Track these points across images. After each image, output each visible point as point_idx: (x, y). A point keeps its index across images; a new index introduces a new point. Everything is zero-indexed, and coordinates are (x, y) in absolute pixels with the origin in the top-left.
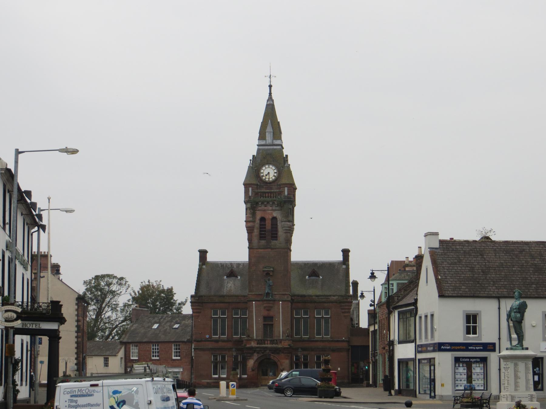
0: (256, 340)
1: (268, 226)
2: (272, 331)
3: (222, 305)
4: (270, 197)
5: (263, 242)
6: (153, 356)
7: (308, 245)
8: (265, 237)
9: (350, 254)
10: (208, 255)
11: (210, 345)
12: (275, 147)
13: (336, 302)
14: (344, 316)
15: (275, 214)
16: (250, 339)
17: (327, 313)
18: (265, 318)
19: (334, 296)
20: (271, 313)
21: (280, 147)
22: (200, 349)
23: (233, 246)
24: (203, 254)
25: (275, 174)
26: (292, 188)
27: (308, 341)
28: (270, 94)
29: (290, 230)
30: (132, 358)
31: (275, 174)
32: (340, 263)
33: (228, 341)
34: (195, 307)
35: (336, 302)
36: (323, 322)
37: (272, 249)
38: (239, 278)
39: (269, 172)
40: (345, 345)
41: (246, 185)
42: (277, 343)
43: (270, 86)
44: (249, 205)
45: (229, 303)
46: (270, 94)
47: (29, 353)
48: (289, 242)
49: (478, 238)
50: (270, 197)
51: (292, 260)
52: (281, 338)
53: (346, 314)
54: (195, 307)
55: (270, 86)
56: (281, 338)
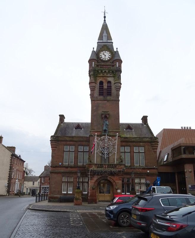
0: (96, 164)
3: (71, 142)
4: (105, 72)
5: (102, 97)
6: (48, 187)
7: (128, 114)
8: (103, 94)
9: (148, 118)
13: (149, 142)
14: (154, 151)
19: (146, 138)
21: (112, 44)
22: (55, 172)
23: (81, 112)
24: (62, 117)
25: (110, 57)
26: (120, 61)
28: (105, 20)
29: (118, 89)
31: (110, 57)
32: (142, 125)
34: (53, 144)
35: (148, 142)
38: (83, 129)
39: (106, 56)
41: (90, 61)
43: (105, 17)
44: (92, 73)
45: (76, 141)
46: (105, 20)
47: (22, 188)
48: (118, 95)
50: (105, 72)
51: (120, 122)
52: (115, 163)
54: (53, 144)
55: (105, 17)
56: (115, 163)
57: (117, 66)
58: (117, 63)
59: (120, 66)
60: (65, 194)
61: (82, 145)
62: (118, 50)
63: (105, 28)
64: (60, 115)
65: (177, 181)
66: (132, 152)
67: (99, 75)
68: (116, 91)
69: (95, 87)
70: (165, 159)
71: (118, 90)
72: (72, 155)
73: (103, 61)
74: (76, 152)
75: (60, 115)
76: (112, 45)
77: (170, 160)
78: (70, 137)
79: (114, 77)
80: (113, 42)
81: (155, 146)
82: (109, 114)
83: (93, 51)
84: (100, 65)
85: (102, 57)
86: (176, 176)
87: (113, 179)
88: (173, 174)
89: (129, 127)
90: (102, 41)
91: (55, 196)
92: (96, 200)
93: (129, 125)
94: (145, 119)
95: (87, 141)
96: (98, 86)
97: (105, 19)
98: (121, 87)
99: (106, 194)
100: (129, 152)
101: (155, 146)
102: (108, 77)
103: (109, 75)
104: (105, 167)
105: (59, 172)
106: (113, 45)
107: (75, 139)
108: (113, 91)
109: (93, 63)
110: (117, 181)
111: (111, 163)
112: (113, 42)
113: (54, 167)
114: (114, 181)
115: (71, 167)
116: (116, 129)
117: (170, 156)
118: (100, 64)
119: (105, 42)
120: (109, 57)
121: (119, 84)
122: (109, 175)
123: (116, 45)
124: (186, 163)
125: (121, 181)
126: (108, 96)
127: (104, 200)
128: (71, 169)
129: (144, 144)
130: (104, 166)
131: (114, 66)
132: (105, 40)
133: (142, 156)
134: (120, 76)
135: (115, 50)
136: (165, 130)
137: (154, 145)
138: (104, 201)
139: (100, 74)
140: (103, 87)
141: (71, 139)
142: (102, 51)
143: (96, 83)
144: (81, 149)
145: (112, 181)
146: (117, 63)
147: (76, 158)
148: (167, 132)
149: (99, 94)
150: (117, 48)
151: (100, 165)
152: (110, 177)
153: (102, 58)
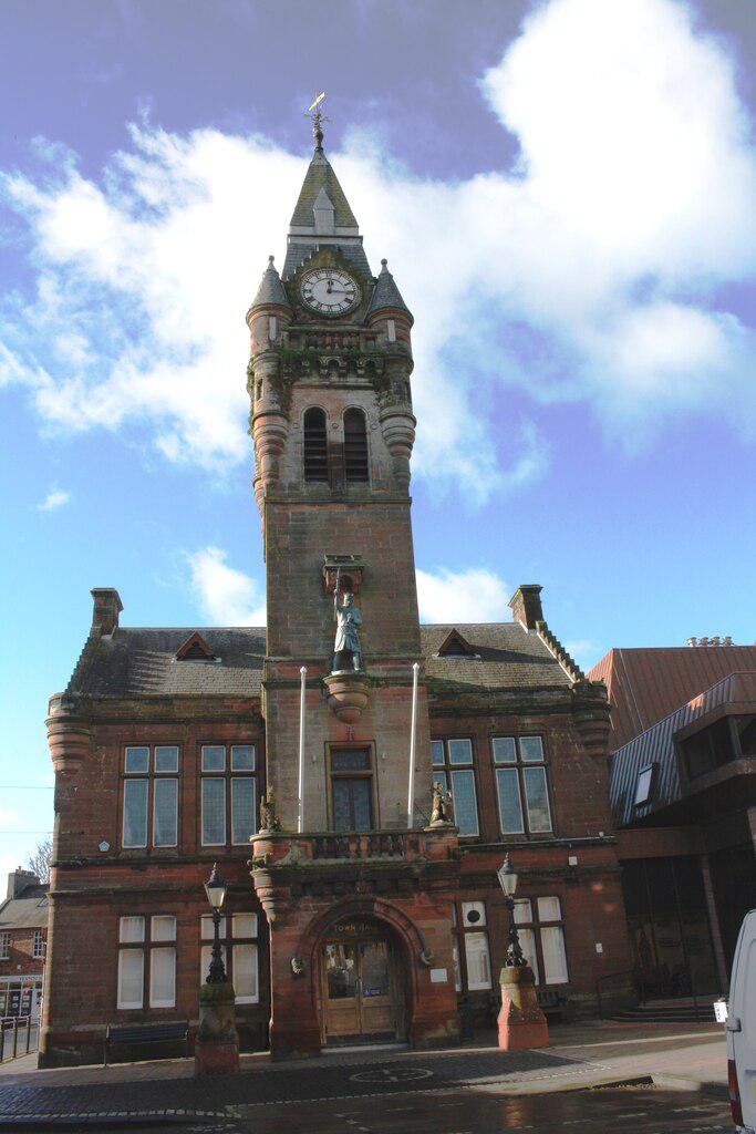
1: (336, 433)
3: (161, 729)
5: (321, 487)
8: (324, 472)
9: (542, 595)
14: (594, 757)
20: (361, 733)
24: (107, 603)
30: (153, 918)
31: (351, 297)
35: (559, 708)
37: (351, 505)
39: (328, 293)
42: (398, 849)
43: (320, 136)
45: (187, 721)
49: (689, 644)
52: (410, 826)
53: (600, 750)
56: (410, 826)
57: (392, 338)
59: (404, 337)
60: (132, 1015)
61: (223, 742)
62: (391, 269)
64: (96, 593)
65: (710, 897)
66: (483, 768)
67: (305, 381)
68: (392, 454)
69: (285, 437)
70: (642, 794)
71: (403, 453)
72: (168, 797)
73: (318, 316)
74: (190, 777)
75: (96, 593)
76: (359, 250)
77: (672, 792)
78: (155, 700)
79: (376, 388)
80: (361, 238)
81: (596, 731)
82: (361, 569)
83: (271, 272)
84: (307, 333)
85: (311, 299)
87: (402, 915)
89: (457, 642)
90: (308, 231)
91: (79, 1028)
92: (316, 1033)
93: (458, 634)
95: (243, 725)
96: (296, 432)
97: (319, 143)
98: (416, 437)
99: (364, 1000)
100: (469, 767)
101: (596, 731)
102: (346, 387)
103: (351, 380)
104: (358, 851)
105: (102, 893)
106: (364, 245)
107: (179, 711)
110: (424, 924)
111: (389, 824)
112: (361, 238)
113: (75, 867)
114: (411, 925)
115: (164, 861)
116: (404, 647)
117: (667, 774)
118: (305, 328)
120: (347, 300)
121: (407, 422)
122: (381, 894)
123: (377, 251)
126: (350, 480)
127: (357, 1032)
128: (164, 874)
129: (540, 719)
130: (353, 847)
131: (374, 339)
132: (324, 223)
133: (535, 782)
134: (407, 384)
135: (376, 271)
137: (593, 725)
138: (354, 1036)
139: (309, 376)
140: (324, 434)
141: (159, 709)
142: (316, 271)
143: (286, 417)
144: (214, 761)
145: (398, 924)
146: (391, 324)
147: (189, 812)
148: (629, 661)
149: (307, 472)
150: (384, 262)
151: (331, 839)
152: (389, 902)
153: (314, 304)
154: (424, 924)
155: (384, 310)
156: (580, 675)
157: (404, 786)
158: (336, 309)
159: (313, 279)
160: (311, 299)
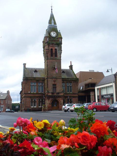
2: (56, 90)
3: (34, 81)
4: (53, 45)
9: (73, 66)
10: (26, 65)
11: (30, 95)
12: (55, 27)
15: (56, 48)
16: (48, 92)
17: (71, 85)
18: (53, 85)
20: (56, 83)
24: (25, 65)
27: (32, 94)
28: (52, 12)
33: (37, 94)
36: (69, 87)
39: (53, 34)
40: (77, 95)
43: (52, 10)
46: (52, 12)
48: (60, 57)
50: (53, 45)
55: (52, 10)
58: (60, 39)
63: (52, 17)
65: (86, 99)
70: (81, 89)
76: (56, 28)
77: (84, 90)
86: (86, 97)
88: (85, 96)
94: (71, 67)
108: (58, 55)
109: (48, 38)
116: (60, 75)
117: (84, 87)
119: (52, 27)
124: (91, 91)
125: (63, 100)
136: (80, 72)
140: (53, 51)
146: (60, 39)
148: (81, 73)
154: (61, 100)
155: (60, 38)
156: (76, 77)
157: (59, 89)
158: (54, 36)
159: (52, 32)
160: (52, 35)
